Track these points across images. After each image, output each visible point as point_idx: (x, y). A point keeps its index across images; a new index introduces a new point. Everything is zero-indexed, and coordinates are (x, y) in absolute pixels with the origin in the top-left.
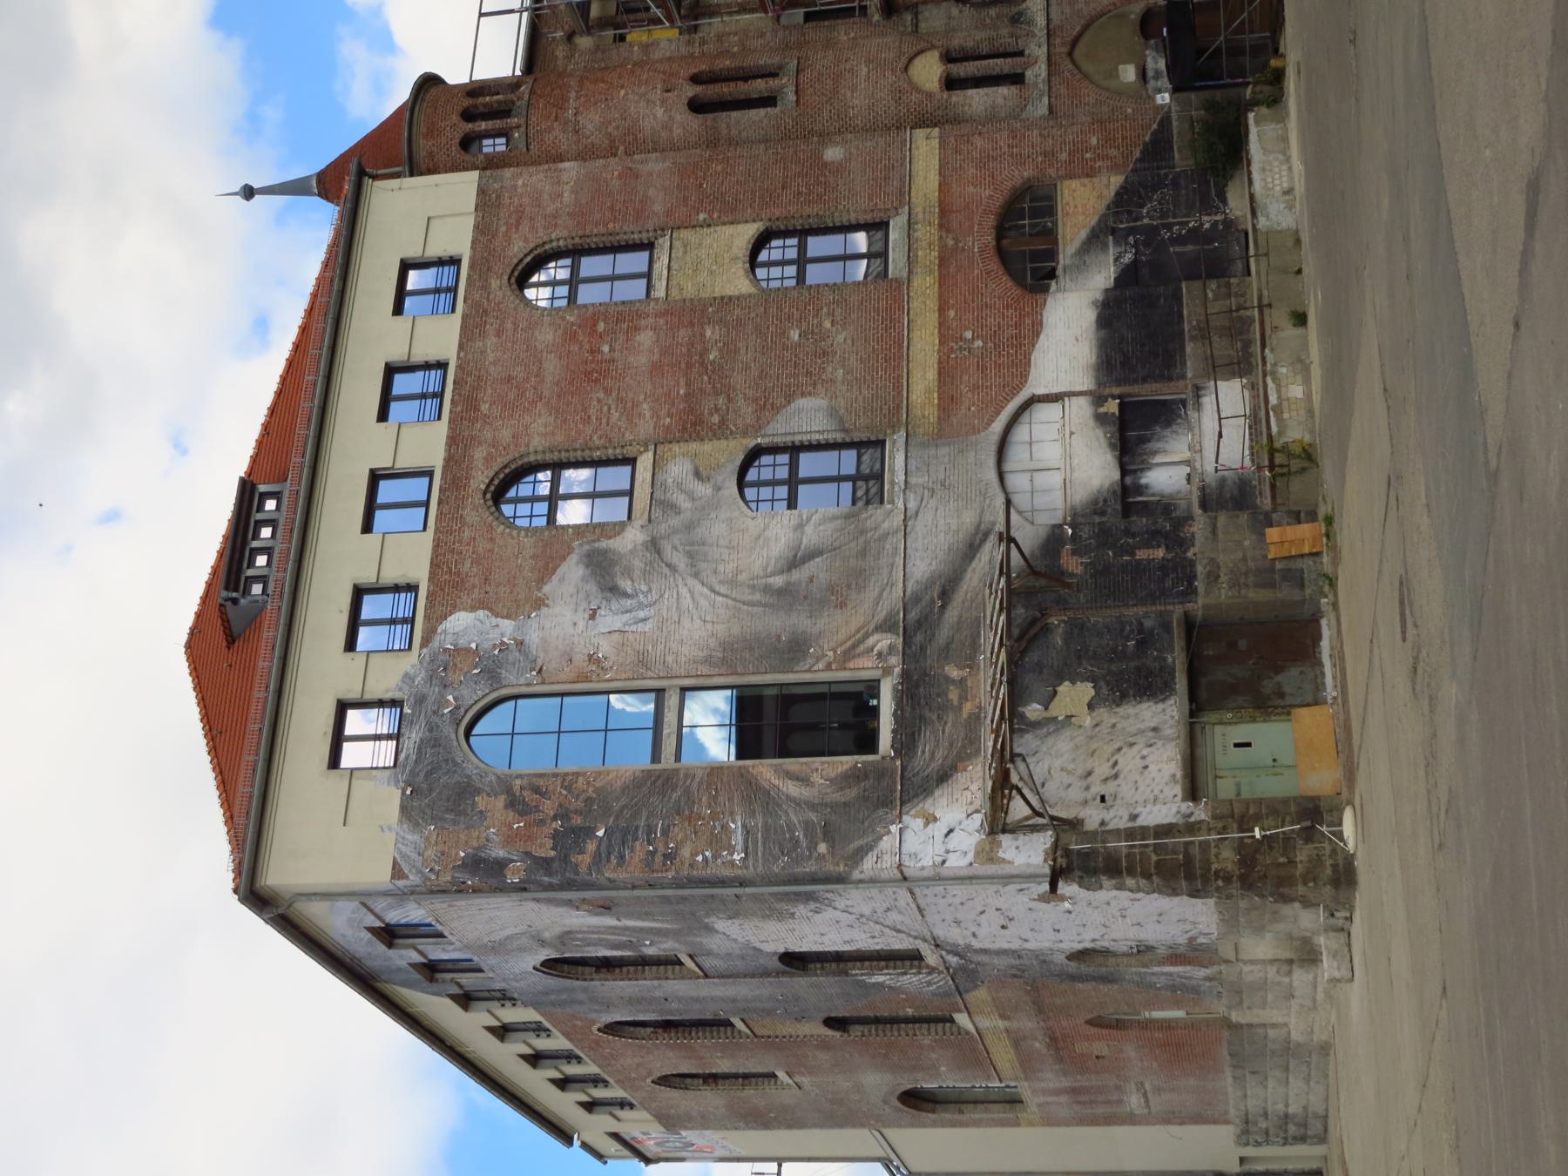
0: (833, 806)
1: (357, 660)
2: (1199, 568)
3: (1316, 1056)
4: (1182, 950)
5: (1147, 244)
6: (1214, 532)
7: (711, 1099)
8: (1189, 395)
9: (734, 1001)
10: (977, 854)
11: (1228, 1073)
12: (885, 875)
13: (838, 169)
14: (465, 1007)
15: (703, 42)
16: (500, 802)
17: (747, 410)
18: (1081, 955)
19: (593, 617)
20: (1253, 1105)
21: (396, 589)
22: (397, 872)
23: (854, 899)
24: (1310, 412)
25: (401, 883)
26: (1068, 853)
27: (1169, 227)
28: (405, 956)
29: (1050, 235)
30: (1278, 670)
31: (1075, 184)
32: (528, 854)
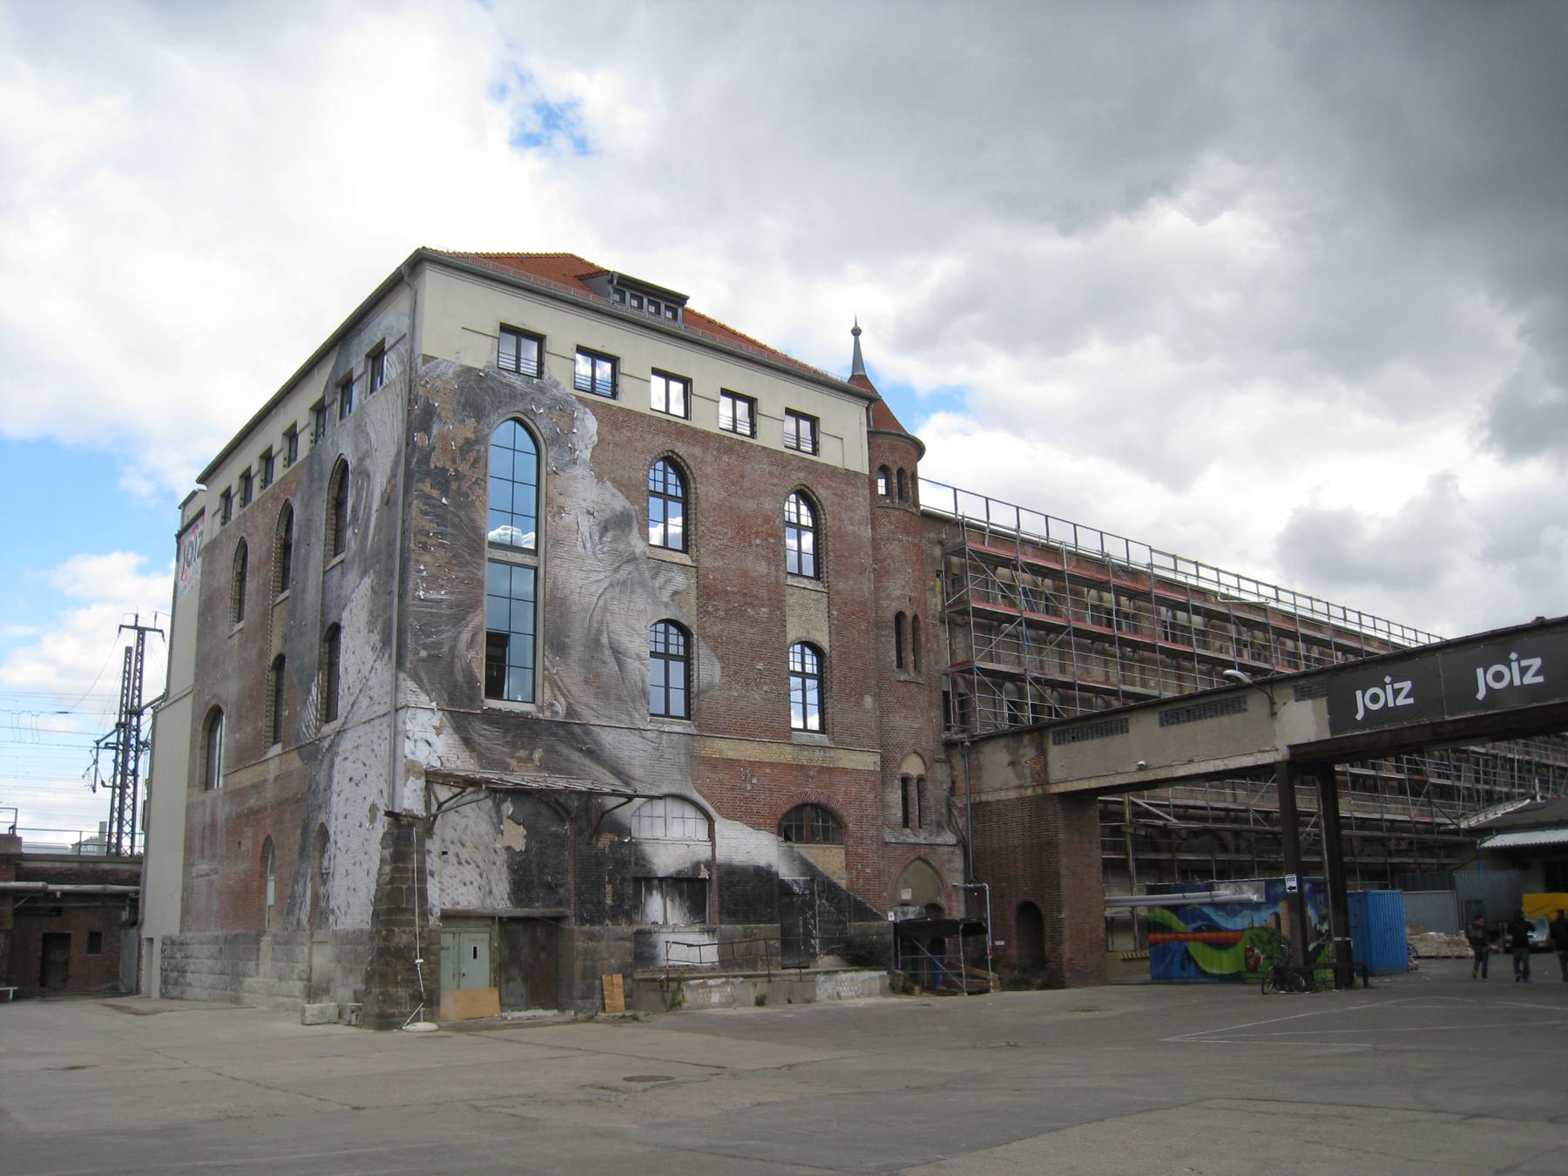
0: (451, 664)
1: (570, 352)
2: (598, 928)
3: (231, 991)
4: (323, 904)
5: (804, 902)
6: (622, 939)
8: (708, 925)
9: (303, 591)
10: (412, 762)
11: (220, 933)
12: (401, 696)
13: (859, 704)
14: (285, 434)
15: (934, 625)
16: (471, 436)
17: (716, 630)
18: (324, 834)
19: (588, 512)
20: (194, 949)
21: (614, 385)
22: (427, 359)
23: (383, 674)
24: (702, 1007)
25: (420, 360)
26: (411, 826)
27: (813, 917)
29: (811, 839)
30: (525, 979)
31: (843, 856)
32: (433, 449)
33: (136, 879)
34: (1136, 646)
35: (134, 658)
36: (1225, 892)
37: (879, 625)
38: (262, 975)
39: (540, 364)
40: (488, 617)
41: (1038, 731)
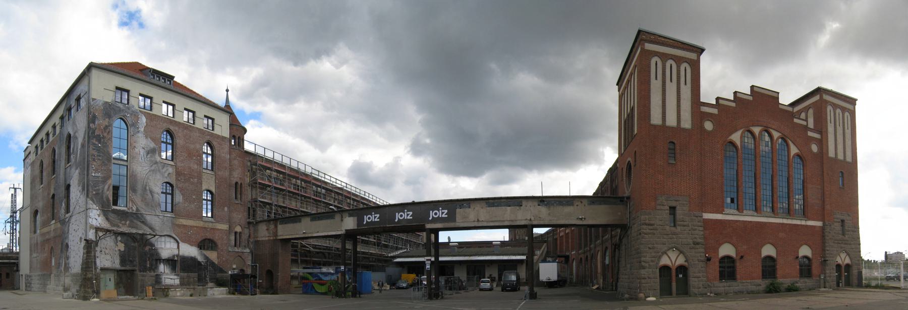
3: (44, 289)
7: (37, 172)
13: (223, 209)
18: (67, 246)
21: (151, 106)
22: (94, 99)
28: (73, 103)
29: (208, 249)
33: (17, 258)
34: (305, 197)
35: (14, 196)
36: (324, 270)
37: (230, 186)
38: (52, 284)
39: (128, 100)
40: (113, 181)
41: (275, 220)
